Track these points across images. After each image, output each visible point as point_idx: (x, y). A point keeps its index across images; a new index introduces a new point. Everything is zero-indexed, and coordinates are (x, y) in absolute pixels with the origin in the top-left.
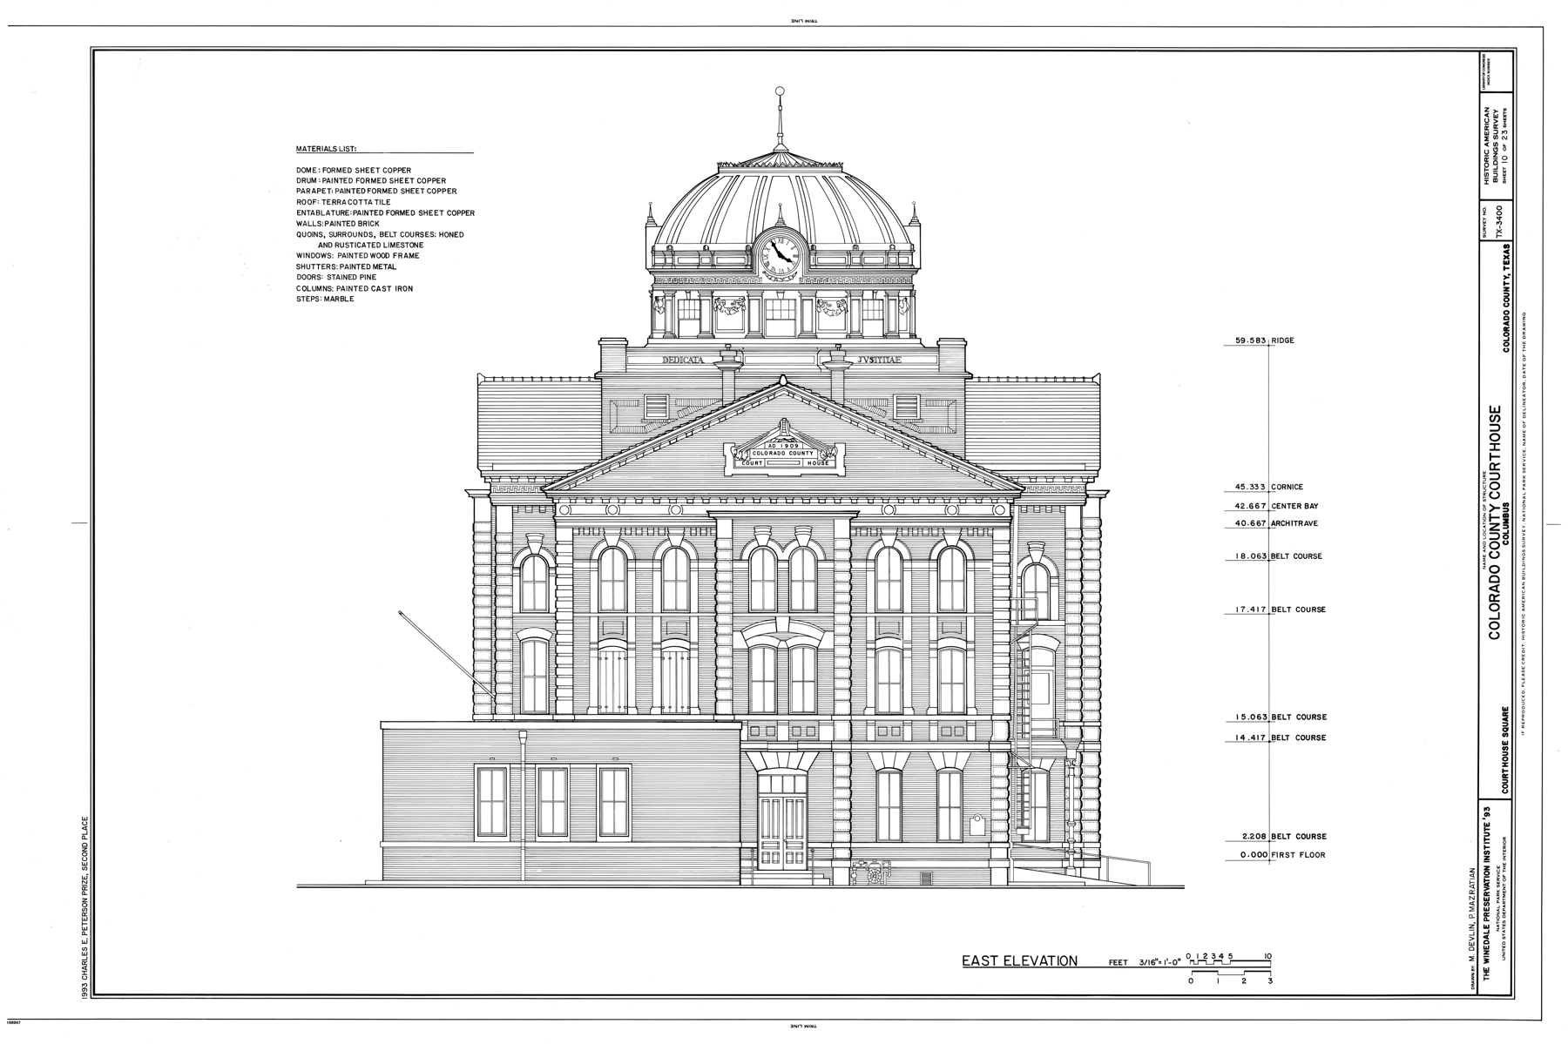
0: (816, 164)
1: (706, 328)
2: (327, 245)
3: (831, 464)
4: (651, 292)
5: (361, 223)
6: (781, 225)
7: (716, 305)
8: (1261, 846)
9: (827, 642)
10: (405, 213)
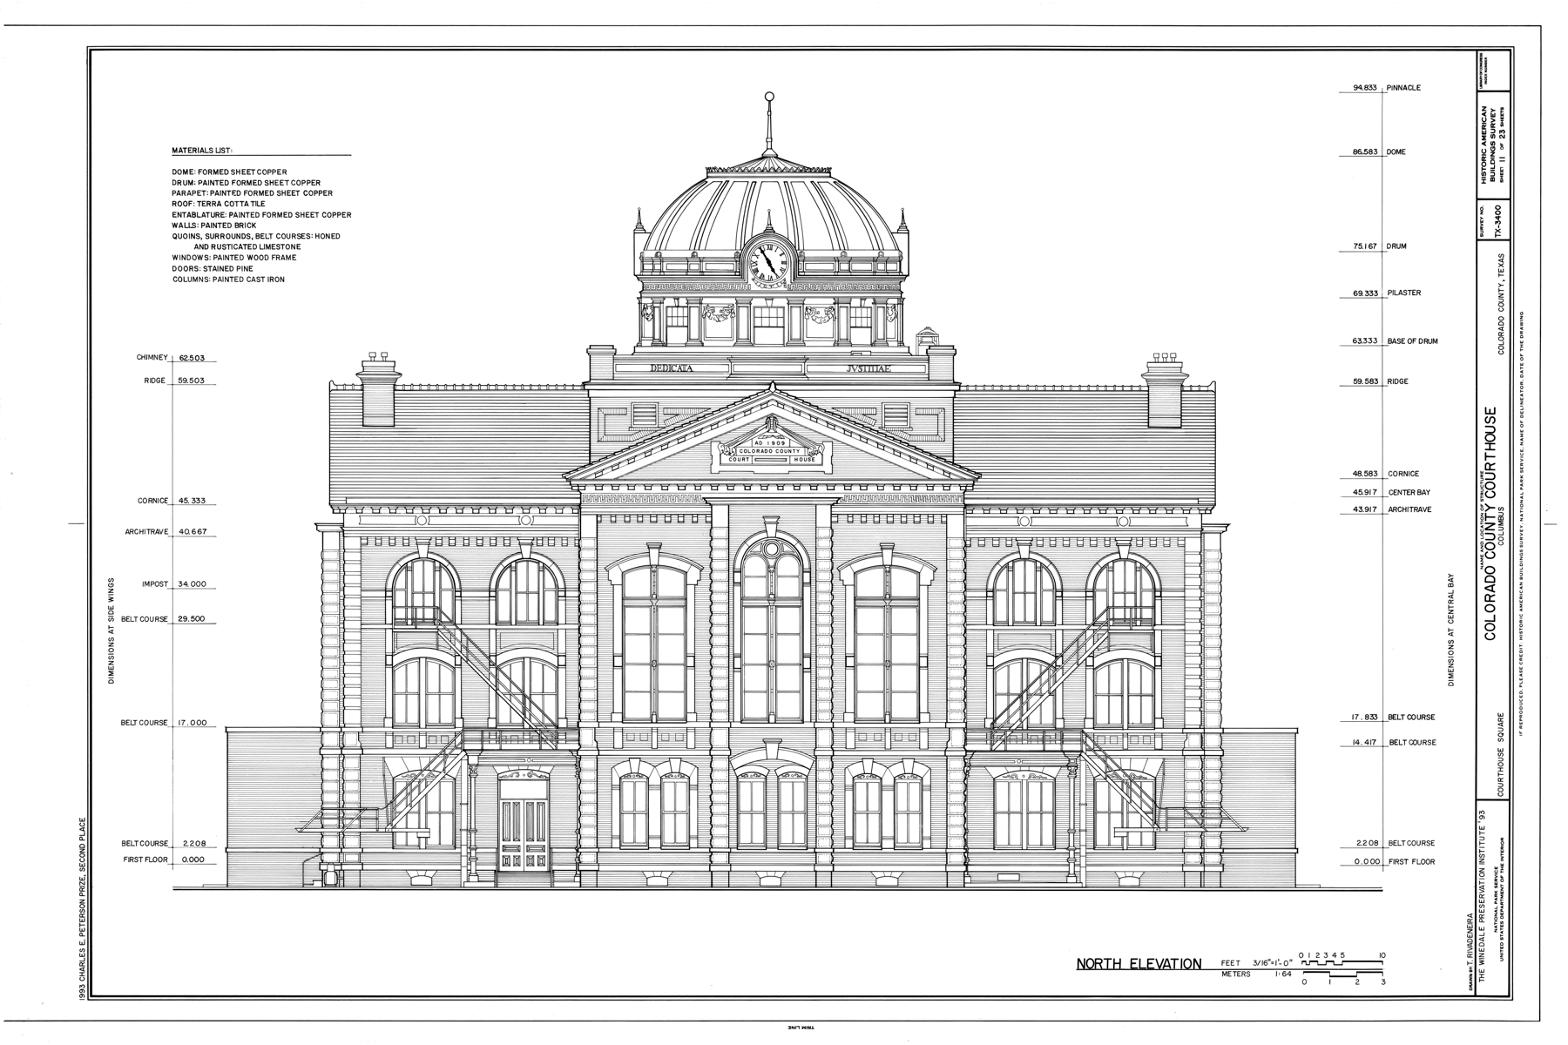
0: (805, 169)
1: (694, 335)
2: (204, 247)
6: (769, 231)
7: (807, 311)
8: (1374, 853)
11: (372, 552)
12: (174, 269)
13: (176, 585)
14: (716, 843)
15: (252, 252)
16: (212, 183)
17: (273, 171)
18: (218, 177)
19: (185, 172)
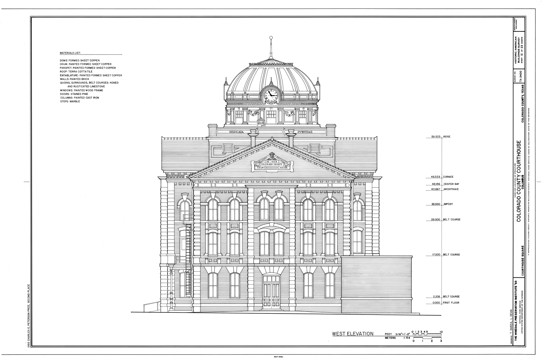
0: (284, 64)
1: (245, 120)
2: (71, 86)
3: (288, 168)
4: (226, 108)
5: (83, 79)
6: (271, 85)
9: (287, 231)
10: (98, 75)
16: (73, 64)
18: (76, 62)
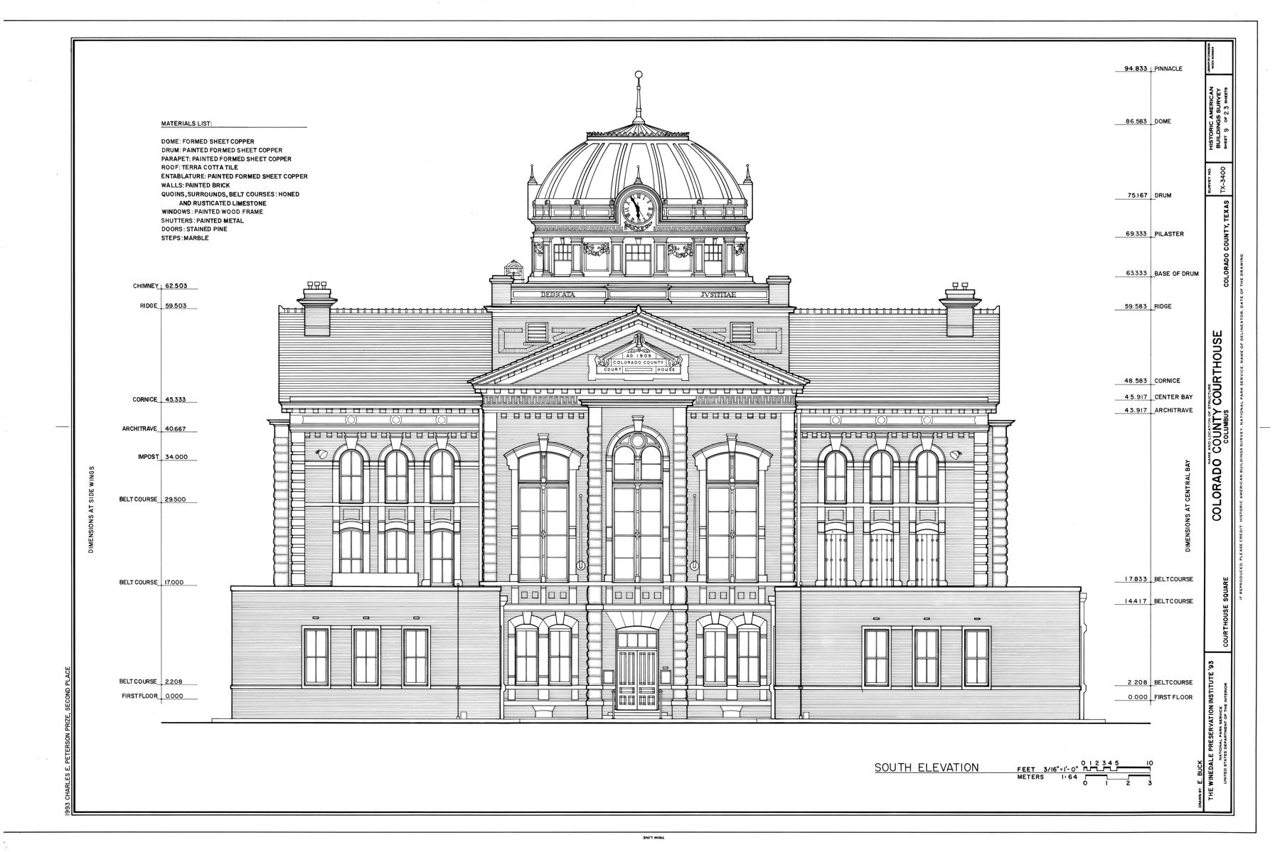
0: (668, 134)
1: (577, 267)
5: (215, 185)
6: (638, 183)
7: (671, 249)
8: (1143, 690)
11: (314, 444)
12: (164, 229)
13: (164, 457)
14: (592, 681)
15: (226, 208)
16: (194, 150)
17: (244, 141)
18: (199, 146)
19: (173, 142)
